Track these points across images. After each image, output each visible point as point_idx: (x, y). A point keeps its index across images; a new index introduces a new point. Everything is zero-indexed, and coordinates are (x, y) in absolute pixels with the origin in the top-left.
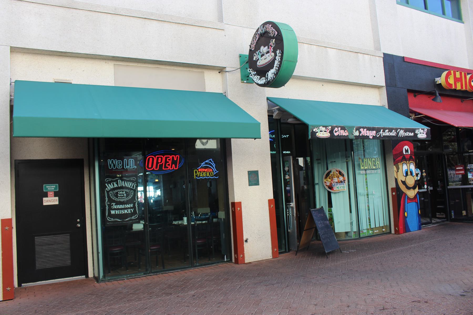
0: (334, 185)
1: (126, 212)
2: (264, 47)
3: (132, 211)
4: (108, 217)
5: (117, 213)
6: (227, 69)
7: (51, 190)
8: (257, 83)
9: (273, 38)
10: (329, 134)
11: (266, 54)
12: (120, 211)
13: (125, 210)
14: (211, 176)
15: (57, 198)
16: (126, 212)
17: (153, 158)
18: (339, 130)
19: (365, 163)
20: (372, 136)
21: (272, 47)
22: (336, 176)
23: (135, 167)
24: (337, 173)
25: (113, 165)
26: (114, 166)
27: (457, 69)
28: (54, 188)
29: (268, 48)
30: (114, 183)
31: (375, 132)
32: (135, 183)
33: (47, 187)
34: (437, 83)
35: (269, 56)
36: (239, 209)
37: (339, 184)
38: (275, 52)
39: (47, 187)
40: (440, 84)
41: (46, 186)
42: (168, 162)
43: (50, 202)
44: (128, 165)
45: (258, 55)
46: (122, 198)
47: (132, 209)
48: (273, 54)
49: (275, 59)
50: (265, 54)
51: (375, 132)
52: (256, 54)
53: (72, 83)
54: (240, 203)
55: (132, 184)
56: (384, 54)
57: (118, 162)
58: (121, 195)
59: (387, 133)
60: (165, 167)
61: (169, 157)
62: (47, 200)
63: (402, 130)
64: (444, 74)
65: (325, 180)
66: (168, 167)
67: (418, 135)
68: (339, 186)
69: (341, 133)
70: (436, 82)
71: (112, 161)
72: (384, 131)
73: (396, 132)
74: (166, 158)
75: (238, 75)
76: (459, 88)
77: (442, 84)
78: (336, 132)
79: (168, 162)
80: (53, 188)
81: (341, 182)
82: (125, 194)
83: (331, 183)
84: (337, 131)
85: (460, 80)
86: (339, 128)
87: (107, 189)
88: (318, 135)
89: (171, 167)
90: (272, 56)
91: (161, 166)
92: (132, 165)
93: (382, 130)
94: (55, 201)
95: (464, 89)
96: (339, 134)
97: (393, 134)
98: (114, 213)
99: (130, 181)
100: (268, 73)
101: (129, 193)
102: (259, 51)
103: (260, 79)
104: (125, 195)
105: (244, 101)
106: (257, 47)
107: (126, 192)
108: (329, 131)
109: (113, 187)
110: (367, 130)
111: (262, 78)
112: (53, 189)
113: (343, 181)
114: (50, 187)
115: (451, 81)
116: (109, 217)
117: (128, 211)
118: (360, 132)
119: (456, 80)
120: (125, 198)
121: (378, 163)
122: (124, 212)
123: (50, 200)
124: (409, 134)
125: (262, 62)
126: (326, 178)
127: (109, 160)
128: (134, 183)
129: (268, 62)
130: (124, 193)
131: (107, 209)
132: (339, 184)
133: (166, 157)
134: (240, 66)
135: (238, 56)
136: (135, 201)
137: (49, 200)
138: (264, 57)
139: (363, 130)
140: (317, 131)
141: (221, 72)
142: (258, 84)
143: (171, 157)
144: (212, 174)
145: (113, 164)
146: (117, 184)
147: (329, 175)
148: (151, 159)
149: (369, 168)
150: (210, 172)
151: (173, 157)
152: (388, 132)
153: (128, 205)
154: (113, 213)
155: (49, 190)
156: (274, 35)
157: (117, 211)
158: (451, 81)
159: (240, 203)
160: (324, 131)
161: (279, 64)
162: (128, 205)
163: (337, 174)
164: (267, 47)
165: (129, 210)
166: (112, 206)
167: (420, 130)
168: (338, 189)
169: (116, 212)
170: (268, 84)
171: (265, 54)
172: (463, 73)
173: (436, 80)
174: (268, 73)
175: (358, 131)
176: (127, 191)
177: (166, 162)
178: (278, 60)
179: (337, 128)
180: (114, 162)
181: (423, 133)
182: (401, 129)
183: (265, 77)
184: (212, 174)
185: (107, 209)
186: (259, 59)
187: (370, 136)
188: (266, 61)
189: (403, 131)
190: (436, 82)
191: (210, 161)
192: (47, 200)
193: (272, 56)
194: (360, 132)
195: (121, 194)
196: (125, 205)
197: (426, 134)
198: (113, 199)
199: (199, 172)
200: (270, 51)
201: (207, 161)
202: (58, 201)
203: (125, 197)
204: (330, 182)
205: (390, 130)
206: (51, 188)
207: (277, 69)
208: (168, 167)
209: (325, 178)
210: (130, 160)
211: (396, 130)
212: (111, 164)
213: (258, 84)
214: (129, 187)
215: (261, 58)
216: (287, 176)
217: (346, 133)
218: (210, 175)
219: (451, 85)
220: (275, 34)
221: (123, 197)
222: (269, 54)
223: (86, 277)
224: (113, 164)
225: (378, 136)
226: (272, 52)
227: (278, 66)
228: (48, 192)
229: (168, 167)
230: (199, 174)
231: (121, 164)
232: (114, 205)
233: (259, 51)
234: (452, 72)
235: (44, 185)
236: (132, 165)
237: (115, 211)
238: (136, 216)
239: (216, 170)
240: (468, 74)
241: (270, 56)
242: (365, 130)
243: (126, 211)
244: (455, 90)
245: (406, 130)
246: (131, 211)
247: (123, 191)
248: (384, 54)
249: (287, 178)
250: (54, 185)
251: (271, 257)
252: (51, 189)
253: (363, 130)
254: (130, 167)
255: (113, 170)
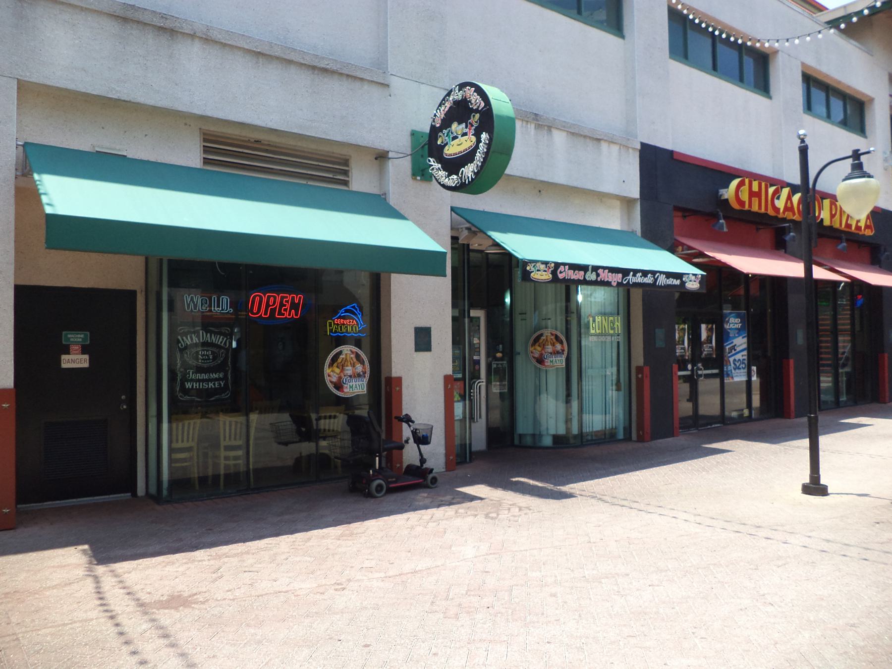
0: (345, 382)
1: (211, 386)
2: (459, 123)
3: (222, 384)
4: (179, 393)
5: (196, 386)
6: (391, 155)
7: (75, 342)
8: (442, 183)
9: (477, 111)
10: (551, 276)
11: (462, 136)
12: (201, 383)
13: (210, 383)
14: (354, 333)
15: (86, 357)
16: (211, 386)
17: (261, 298)
18: (566, 270)
19: (597, 324)
20: (616, 282)
21: (472, 126)
22: (551, 343)
23: (231, 311)
24: (552, 337)
25: (194, 304)
26: (195, 306)
27: (754, 176)
28: (82, 338)
29: (466, 127)
30: (193, 335)
31: (620, 275)
32: (228, 337)
33: (69, 336)
34: (722, 198)
35: (466, 141)
36: (398, 389)
37: (354, 380)
38: (478, 135)
39: (69, 336)
40: (727, 200)
41: (66, 335)
42: (285, 305)
43: (74, 363)
44: (218, 306)
45: (446, 136)
46: (206, 361)
47: (221, 382)
48: (474, 139)
49: (477, 147)
50: (460, 136)
51: (620, 275)
52: (444, 134)
53: (126, 156)
54: (399, 379)
55: (223, 339)
56: (643, 144)
57: (202, 300)
58: (204, 357)
59: (639, 278)
60: (280, 313)
61: (287, 297)
62: (69, 360)
63: (662, 275)
64: (735, 183)
65: (532, 349)
66: (283, 314)
67: (686, 284)
68: (354, 383)
69: (569, 275)
70: (721, 195)
71: (192, 299)
72: (634, 275)
73: (654, 277)
74: (282, 298)
75: (406, 164)
76: (755, 208)
77: (730, 201)
78: (561, 272)
79: (285, 305)
80: (80, 338)
81: (558, 352)
82: (211, 356)
83: (340, 378)
84: (563, 272)
85: (758, 195)
86: (567, 267)
87: (180, 345)
88: (533, 276)
89: (289, 315)
90: (472, 143)
91: (273, 311)
92: (225, 307)
93: (632, 273)
94: (83, 362)
95: (763, 210)
96: (565, 277)
97: (649, 280)
98: (190, 387)
99: (221, 334)
100: (463, 171)
101: (217, 353)
102: (448, 129)
103: (448, 177)
104: (211, 358)
105: (415, 211)
106: (447, 122)
107: (213, 353)
108: (550, 270)
109: (191, 342)
110: (609, 272)
111: (452, 177)
112: (81, 340)
113: (361, 373)
114: (73, 336)
115: (745, 196)
116: (181, 394)
117: (214, 384)
118: (598, 275)
119: (752, 194)
120: (210, 362)
121: (617, 325)
122: (208, 386)
123: (73, 360)
124: (672, 282)
125: (453, 149)
126: (534, 344)
127: (186, 297)
128: (227, 337)
129: (464, 152)
130: (210, 353)
131: (179, 379)
132: (354, 380)
133: (268, 296)
134: (412, 151)
135: (409, 133)
136: (228, 368)
137: (72, 359)
138: (456, 141)
139: (603, 272)
140: (533, 269)
141: (379, 159)
142: (444, 186)
143: (289, 298)
144: (356, 329)
145: (193, 302)
146: (198, 337)
147: (538, 341)
148: (257, 299)
149: (603, 332)
150: (353, 325)
151: (293, 298)
152: (641, 277)
153: (216, 374)
154: (189, 387)
155: (72, 342)
156: (479, 107)
157: (196, 384)
158: (745, 196)
159: (399, 379)
160: (544, 271)
161: (484, 156)
162: (216, 374)
163: (552, 339)
164: (464, 125)
165: (216, 383)
166: (188, 375)
167: (691, 275)
168: (552, 364)
169: (195, 385)
170: (461, 188)
171: (460, 136)
172: (763, 184)
173: (720, 193)
174: (463, 171)
175: (594, 273)
176: (215, 350)
177: (282, 305)
178: (483, 150)
179: (563, 267)
180: (195, 300)
181: (695, 281)
182: (661, 272)
183: (457, 174)
184: (356, 329)
185: (179, 379)
186: (449, 143)
187: (613, 281)
188: (461, 148)
189: (664, 276)
190: (721, 195)
191: (353, 307)
192: (69, 360)
193: (472, 141)
194: (598, 275)
195: (204, 355)
196: (211, 374)
197: (700, 283)
198: (190, 362)
199: (334, 324)
200: (469, 134)
201: (348, 307)
202: (88, 361)
203: (211, 361)
204: (539, 351)
205: (645, 273)
206: (76, 338)
207: (480, 164)
208: (284, 313)
209: (532, 346)
210: (223, 298)
211: (654, 273)
212: (190, 302)
213: (444, 186)
214: (219, 343)
215: (452, 143)
216: (476, 339)
217: (576, 275)
218: (352, 330)
219: (742, 203)
220: (481, 105)
221: (207, 360)
222: (466, 137)
223: (132, 495)
224: (193, 302)
225: (625, 283)
226: (472, 135)
227: (482, 160)
228: (70, 345)
229: (284, 313)
230: (335, 328)
231: (206, 303)
232: (191, 373)
233: (449, 130)
234: (747, 181)
235: (64, 333)
236: (225, 307)
237: (192, 383)
238: (228, 394)
239: (361, 322)
240: (772, 185)
241: (468, 141)
242: (607, 271)
243: (211, 385)
244: (749, 212)
245: (669, 275)
246: (220, 385)
247: (207, 351)
248: (643, 144)
249: (475, 342)
250: (83, 334)
251: (444, 470)
252: (76, 339)
253: (603, 272)
254: (222, 310)
255: (193, 313)
